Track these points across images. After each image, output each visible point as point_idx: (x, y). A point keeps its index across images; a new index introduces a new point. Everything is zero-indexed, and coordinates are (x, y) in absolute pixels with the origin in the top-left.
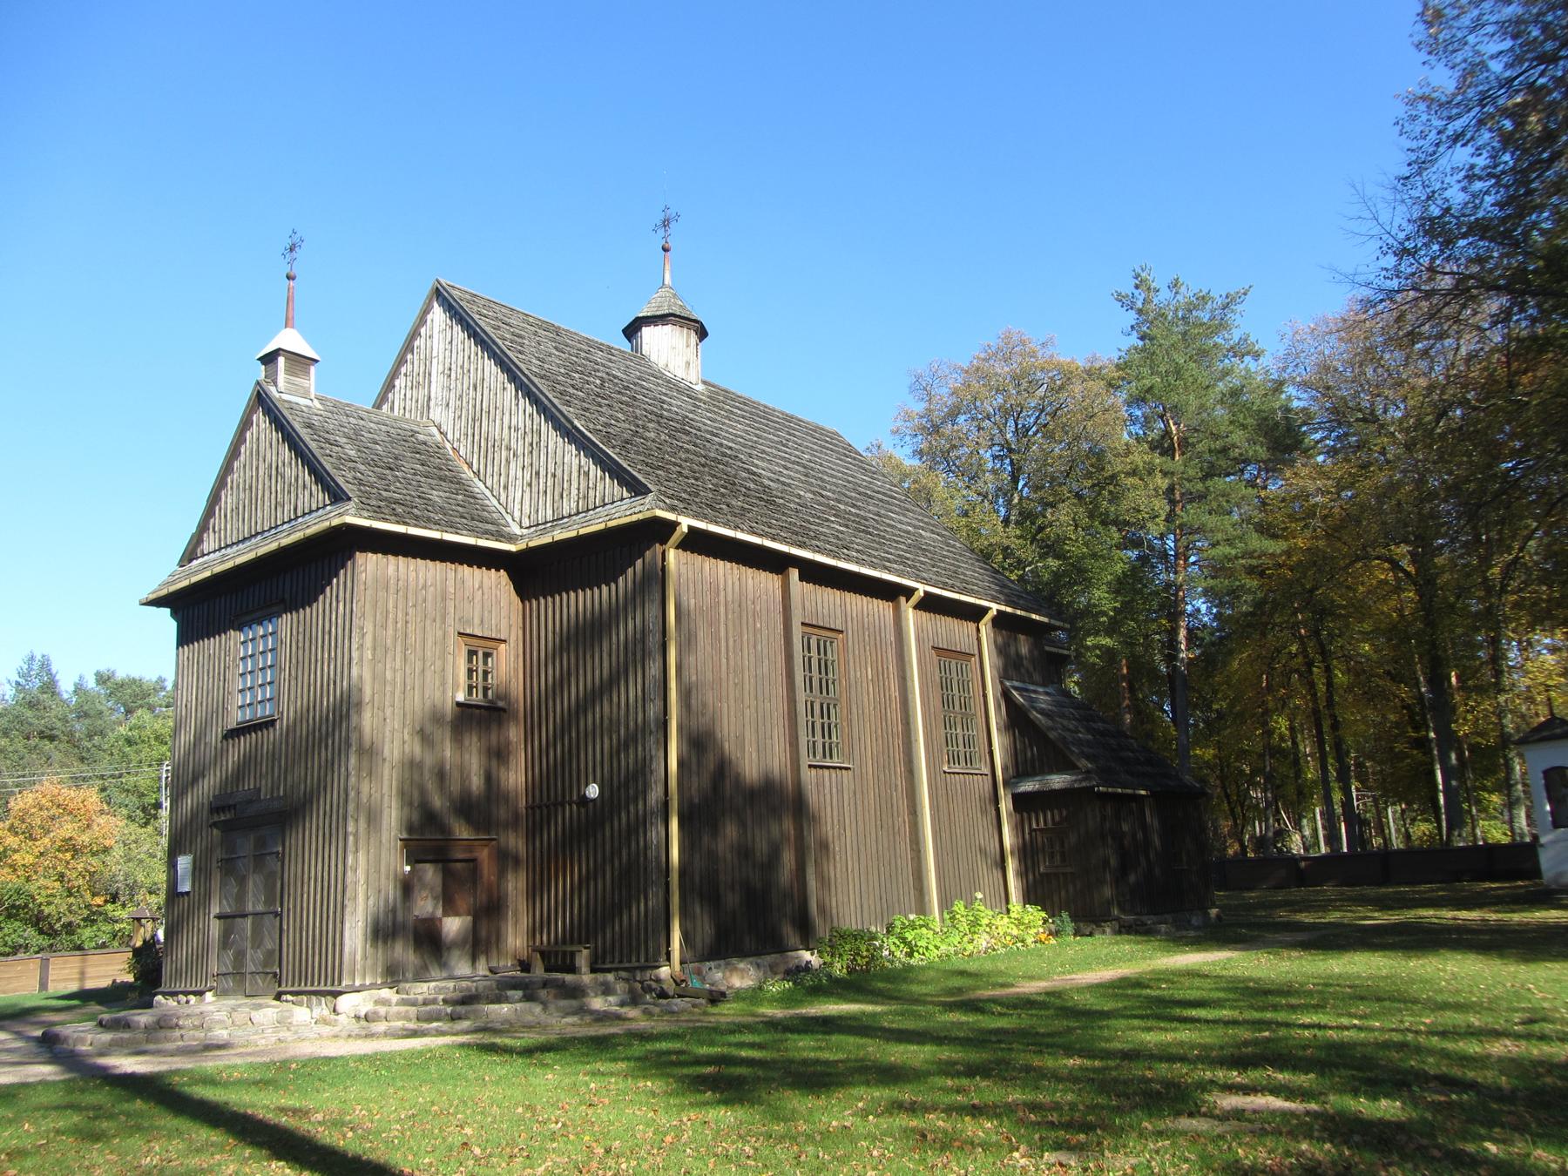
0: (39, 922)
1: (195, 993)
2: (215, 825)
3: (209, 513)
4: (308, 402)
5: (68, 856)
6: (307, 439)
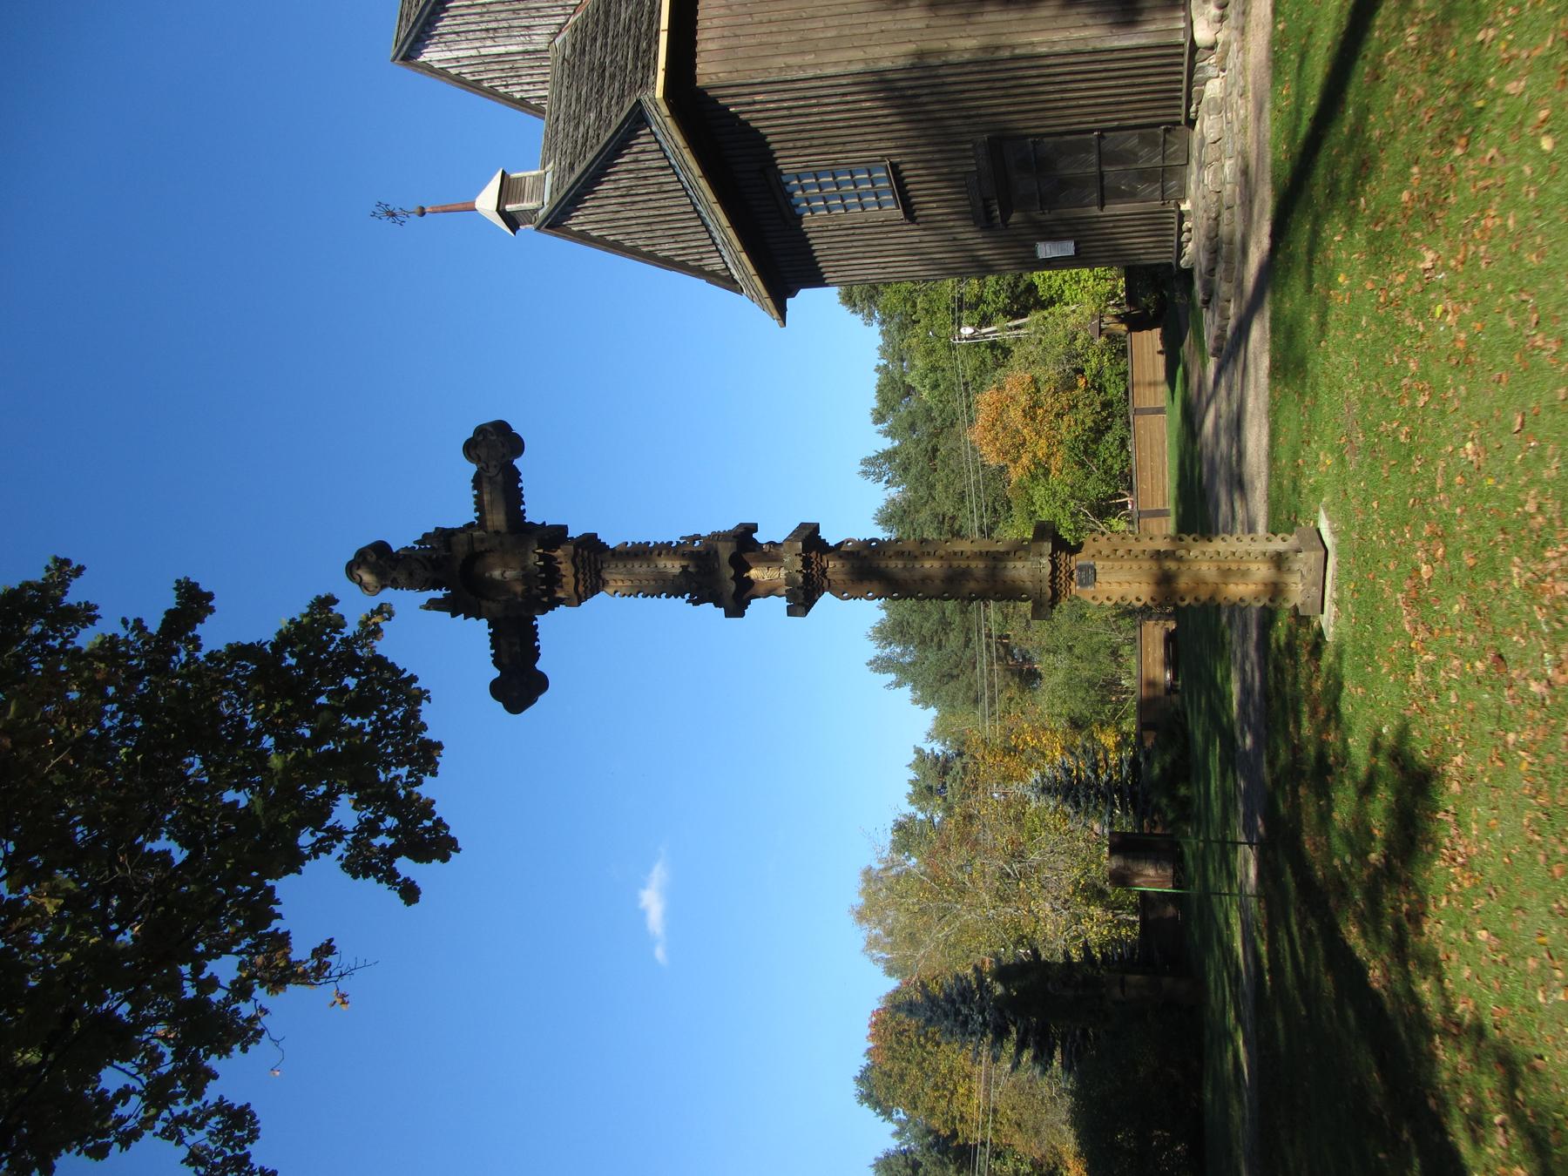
0: (1099, 432)
1: (1181, 223)
2: (1005, 221)
3: (682, 267)
4: (549, 175)
5: (1040, 411)
6: (584, 165)
